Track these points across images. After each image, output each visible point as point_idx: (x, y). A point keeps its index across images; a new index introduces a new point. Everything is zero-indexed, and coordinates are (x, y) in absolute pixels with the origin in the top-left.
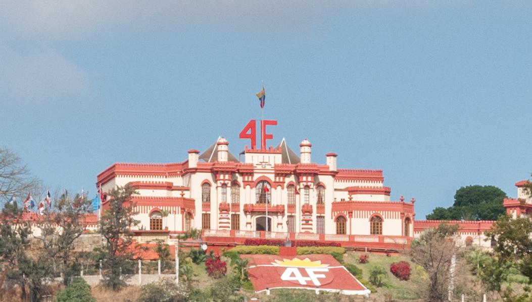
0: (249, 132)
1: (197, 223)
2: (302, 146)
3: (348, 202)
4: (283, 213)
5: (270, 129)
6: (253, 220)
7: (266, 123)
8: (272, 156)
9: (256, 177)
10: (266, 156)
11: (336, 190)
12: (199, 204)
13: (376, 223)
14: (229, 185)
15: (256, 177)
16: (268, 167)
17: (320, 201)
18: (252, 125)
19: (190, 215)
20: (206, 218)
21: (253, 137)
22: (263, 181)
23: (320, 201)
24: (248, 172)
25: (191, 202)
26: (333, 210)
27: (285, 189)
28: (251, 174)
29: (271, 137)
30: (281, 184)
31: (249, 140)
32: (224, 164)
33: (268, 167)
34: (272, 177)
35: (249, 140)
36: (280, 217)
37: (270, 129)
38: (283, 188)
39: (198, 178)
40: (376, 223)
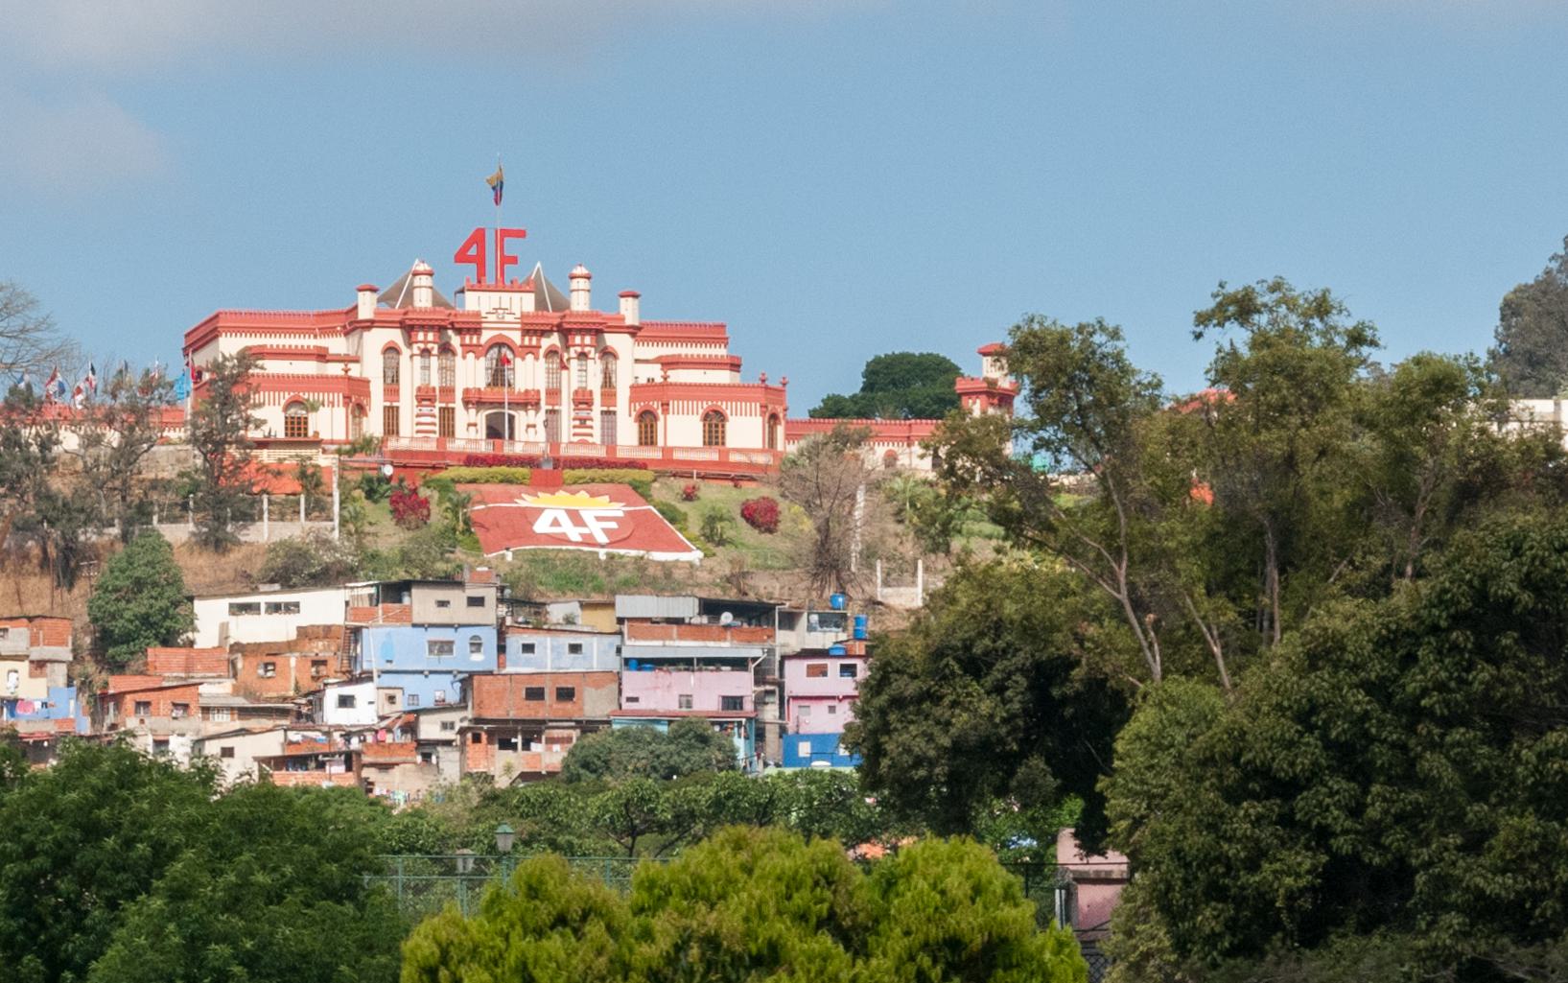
0: (473, 251)
1: (373, 425)
2: (572, 277)
3: (661, 385)
5: (512, 246)
6: (481, 418)
7: (505, 233)
8: (516, 296)
9: (486, 336)
10: (505, 296)
12: (377, 389)
13: (714, 425)
14: (435, 351)
15: (486, 336)
16: (508, 318)
17: (608, 382)
18: (478, 238)
19: (360, 410)
20: (391, 415)
21: (480, 261)
23: (608, 382)
24: (471, 327)
26: (632, 400)
27: (542, 360)
28: (477, 330)
29: (514, 260)
30: (533, 350)
31: (473, 266)
32: (425, 311)
33: (508, 318)
34: (516, 337)
35: (473, 266)
36: (532, 413)
37: (512, 246)
38: (537, 358)
39: (377, 339)
40: (714, 425)
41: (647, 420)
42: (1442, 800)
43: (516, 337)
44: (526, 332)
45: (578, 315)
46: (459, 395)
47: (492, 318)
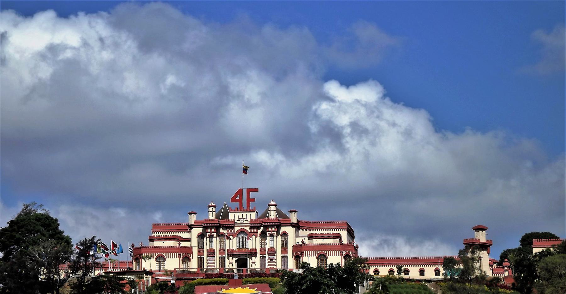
0: (238, 197)
1: (194, 264)
2: (209, 207)
3: (301, 245)
4: (256, 255)
5: (253, 195)
6: (233, 260)
7: (249, 191)
8: (248, 214)
9: (236, 229)
10: (244, 214)
11: (190, 241)
12: (195, 251)
13: (322, 257)
14: (215, 236)
15: (236, 229)
16: (246, 222)
17: (284, 246)
18: (240, 192)
19: (187, 259)
20: (201, 261)
21: (240, 201)
22: (242, 232)
23: (284, 246)
24: (230, 227)
25: (190, 249)
26: (293, 252)
27: (258, 238)
28: (233, 228)
29: (254, 200)
30: (255, 234)
31: (238, 203)
32: (213, 220)
33: (246, 222)
34: (248, 229)
35: (238, 203)
36: (253, 258)
37: (253, 195)
38: (256, 237)
39: (197, 231)
40: (322, 257)
41: (297, 258)
42: (14, 230)
43: (248, 229)
44: (251, 227)
45: (272, 219)
46: (259, 255)
47: (239, 222)
